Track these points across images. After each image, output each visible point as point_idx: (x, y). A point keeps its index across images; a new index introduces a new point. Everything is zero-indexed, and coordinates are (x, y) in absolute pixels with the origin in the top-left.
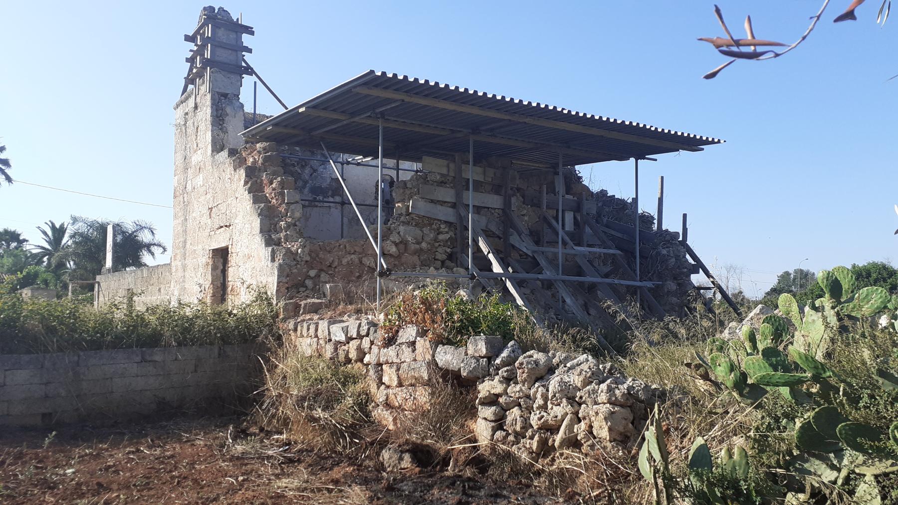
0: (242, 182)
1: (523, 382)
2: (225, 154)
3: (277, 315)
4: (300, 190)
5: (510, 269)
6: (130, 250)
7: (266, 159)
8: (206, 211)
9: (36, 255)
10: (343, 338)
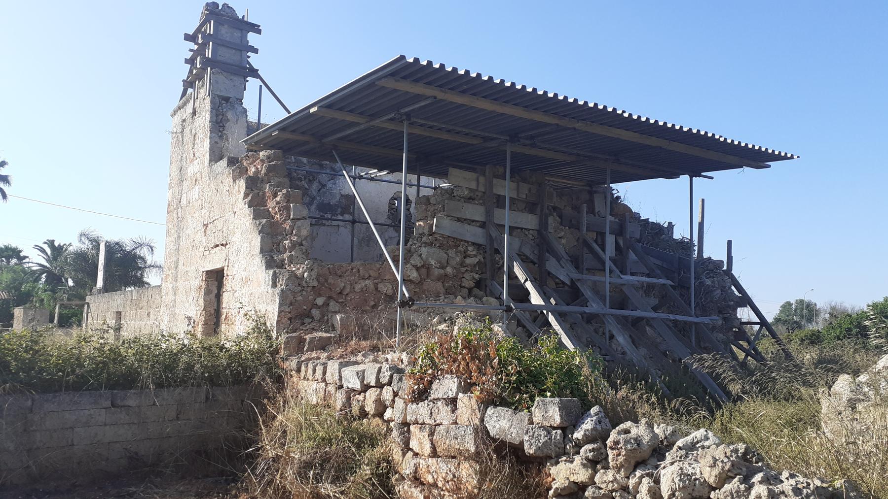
0: (242, 195)
1: (618, 469)
2: (223, 163)
3: (277, 351)
4: (309, 205)
5: (553, 301)
6: (125, 268)
7: (270, 169)
8: (200, 228)
9: (34, 272)
10: (357, 385)
